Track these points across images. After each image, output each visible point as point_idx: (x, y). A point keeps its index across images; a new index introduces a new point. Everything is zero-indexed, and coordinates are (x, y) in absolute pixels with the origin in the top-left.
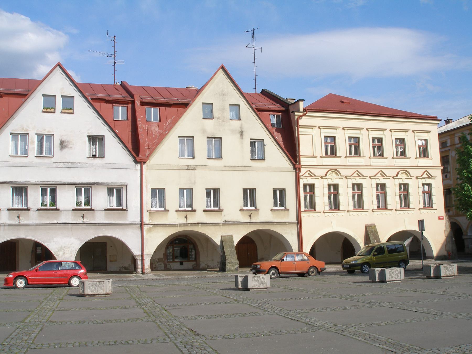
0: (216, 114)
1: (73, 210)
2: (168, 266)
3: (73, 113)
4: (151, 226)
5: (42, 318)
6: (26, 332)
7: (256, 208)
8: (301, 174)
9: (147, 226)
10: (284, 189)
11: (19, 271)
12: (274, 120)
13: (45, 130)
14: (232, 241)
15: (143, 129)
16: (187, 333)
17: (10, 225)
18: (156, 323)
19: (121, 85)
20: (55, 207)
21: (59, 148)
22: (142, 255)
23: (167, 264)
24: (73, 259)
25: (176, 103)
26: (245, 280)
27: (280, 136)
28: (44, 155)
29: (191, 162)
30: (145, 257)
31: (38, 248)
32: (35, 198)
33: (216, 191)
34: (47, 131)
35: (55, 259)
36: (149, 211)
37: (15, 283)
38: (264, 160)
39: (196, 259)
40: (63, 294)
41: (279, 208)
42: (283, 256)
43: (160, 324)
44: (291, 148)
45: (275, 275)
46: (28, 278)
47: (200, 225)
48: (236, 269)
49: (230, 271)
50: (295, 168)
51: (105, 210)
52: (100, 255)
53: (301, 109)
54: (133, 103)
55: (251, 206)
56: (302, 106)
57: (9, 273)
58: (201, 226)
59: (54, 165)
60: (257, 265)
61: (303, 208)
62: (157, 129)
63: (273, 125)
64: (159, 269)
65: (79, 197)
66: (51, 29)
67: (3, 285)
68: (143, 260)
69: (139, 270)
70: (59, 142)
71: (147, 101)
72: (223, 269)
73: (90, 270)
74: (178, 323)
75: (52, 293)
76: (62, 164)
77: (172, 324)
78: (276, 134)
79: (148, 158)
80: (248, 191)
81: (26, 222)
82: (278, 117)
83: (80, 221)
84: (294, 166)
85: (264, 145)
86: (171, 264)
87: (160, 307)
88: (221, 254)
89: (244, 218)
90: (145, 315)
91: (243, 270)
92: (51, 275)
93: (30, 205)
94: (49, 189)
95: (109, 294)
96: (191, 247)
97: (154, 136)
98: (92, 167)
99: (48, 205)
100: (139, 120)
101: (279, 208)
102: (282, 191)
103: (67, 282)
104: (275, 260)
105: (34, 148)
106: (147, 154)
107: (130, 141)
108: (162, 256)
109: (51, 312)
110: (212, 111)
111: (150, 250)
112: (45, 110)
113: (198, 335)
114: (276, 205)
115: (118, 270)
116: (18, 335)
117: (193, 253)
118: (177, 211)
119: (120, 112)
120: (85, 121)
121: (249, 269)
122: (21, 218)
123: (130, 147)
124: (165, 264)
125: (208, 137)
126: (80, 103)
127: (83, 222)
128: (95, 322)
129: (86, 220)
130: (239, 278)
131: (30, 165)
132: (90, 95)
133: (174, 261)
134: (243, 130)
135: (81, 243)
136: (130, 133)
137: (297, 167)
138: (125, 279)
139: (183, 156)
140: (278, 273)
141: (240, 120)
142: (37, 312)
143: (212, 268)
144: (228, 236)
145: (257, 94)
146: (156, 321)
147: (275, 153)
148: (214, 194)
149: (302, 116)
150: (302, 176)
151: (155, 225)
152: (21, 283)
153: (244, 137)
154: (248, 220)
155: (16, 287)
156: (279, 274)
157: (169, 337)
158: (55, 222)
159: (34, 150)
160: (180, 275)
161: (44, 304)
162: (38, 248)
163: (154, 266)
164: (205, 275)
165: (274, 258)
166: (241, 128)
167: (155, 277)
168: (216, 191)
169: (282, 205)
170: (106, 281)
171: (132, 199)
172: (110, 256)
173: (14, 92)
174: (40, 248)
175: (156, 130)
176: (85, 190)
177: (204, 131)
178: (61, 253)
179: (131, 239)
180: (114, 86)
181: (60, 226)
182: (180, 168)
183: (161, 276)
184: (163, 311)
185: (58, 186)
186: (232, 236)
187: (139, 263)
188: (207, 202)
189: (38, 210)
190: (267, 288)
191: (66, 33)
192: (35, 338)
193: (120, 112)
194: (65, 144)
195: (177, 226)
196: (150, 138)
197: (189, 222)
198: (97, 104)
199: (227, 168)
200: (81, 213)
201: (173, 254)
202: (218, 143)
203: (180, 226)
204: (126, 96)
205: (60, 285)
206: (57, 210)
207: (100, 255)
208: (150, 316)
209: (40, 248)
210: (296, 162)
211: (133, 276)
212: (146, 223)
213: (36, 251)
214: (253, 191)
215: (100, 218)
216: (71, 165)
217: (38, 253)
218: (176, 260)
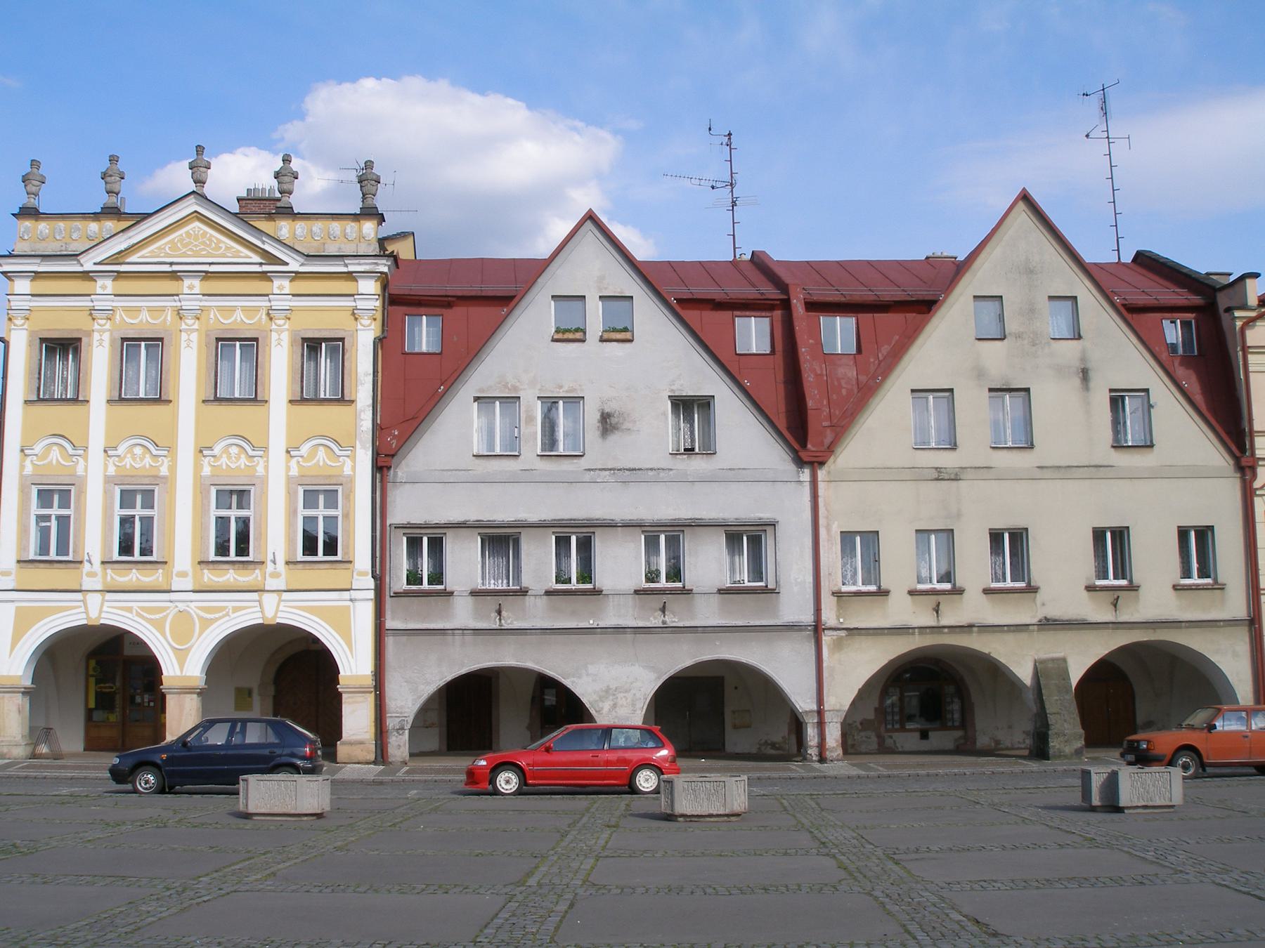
0: (1012, 326)
1: (637, 592)
2: (889, 742)
3: (631, 341)
4: (843, 633)
5: (570, 875)
6: (533, 910)
7: (1131, 581)
8: (1256, 485)
9: (831, 633)
10: (1211, 528)
11: (499, 750)
12: (1173, 332)
13: (561, 387)
14: (1065, 675)
15: (816, 375)
16: (963, 928)
17: (476, 631)
18: (876, 898)
19: (752, 260)
20: (679, 585)
21: (598, 433)
22: (820, 713)
23: (886, 735)
24: (638, 720)
25: (900, 301)
26: (1112, 784)
27: (1194, 378)
28: (561, 449)
29: (947, 460)
30: (828, 717)
31: (547, 691)
32: (539, 563)
33: (1019, 537)
34: (566, 388)
35: (591, 718)
36: (838, 594)
37: (492, 781)
38: (1151, 446)
39: (966, 722)
40: (617, 813)
41: (1195, 580)
42: (1215, 717)
43: (887, 900)
44: (1225, 409)
45: (1191, 771)
46: (527, 768)
48: (1078, 752)
49: (1059, 757)
50: (1240, 468)
51: (721, 591)
52: (708, 709)
53: (1252, 300)
54: (786, 305)
55: (1115, 578)
56: (1254, 291)
57: (479, 755)
58: (979, 632)
59: (588, 476)
60: (1138, 741)
62: (852, 373)
63: (1173, 347)
64: (863, 748)
65: (653, 559)
66: (580, 124)
67: (461, 787)
68: (821, 725)
69: (813, 752)
70: (598, 416)
71: (822, 299)
72: (1040, 750)
73: (688, 749)
74: (934, 899)
75: (588, 810)
77: (919, 903)
78: (1180, 372)
79: (831, 449)
80: (1108, 535)
81: (516, 625)
82: (1186, 325)
83: (655, 620)
84: (1237, 460)
85: (1150, 406)
86: (895, 735)
87: (879, 852)
88: (1035, 708)
89: (1098, 612)
90: (843, 874)
91: (1096, 755)
92: (586, 763)
93: (526, 581)
94: (425, 540)
95: (738, 815)
96: (950, 689)
97: (844, 392)
99: (574, 579)
100: (803, 350)
101: (1195, 580)
102: (1205, 534)
103: (626, 781)
104: (1191, 727)
106: (827, 441)
107: (782, 407)
108: (870, 715)
109: (592, 861)
110: (1001, 318)
111: (841, 696)
112: (559, 336)
113: (995, 934)
114: (1187, 573)
115: (754, 751)
116: (514, 920)
117: (956, 706)
118: (912, 593)
119: (753, 334)
120: (665, 356)
121: (1115, 754)
122: (504, 613)
123: (782, 424)
124: (879, 736)
125: (991, 390)
126: (649, 316)
127: (664, 622)
128: (709, 890)
129: (672, 620)
130: (1094, 777)
131: (526, 478)
132: (676, 290)
133: (903, 729)
134: (1089, 365)
135: (659, 678)
136: (781, 387)
138: (775, 775)
139: (924, 443)
140: (1201, 764)
141: (1080, 337)
142: (555, 858)
143: (1007, 749)
144: (1053, 660)
145: (1124, 264)
146: (876, 893)
147: (1181, 429)
148: (1011, 544)
149: (1253, 320)
151: (853, 631)
152: (507, 782)
153: (1092, 384)
154: (1106, 615)
155: (496, 792)
156: (1203, 765)
157: (915, 938)
158: (591, 623)
160: (922, 766)
161: (570, 837)
162: (547, 691)
163: (850, 742)
164: (991, 769)
165: (1187, 722)
167: (855, 772)
168: (1019, 537)
169: (1203, 573)
170: (731, 781)
171: (790, 563)
172: (734, 712)
173: (479, 294)
174: (554, 691)
175: (850, 375)
176: (668, 536)
177: (980, 373)
178: (606, 706)
179: (788, 670)
180: (734, 263)
182: (917, 475)
183: (870, 769)
184: (890, 865)
185: (598, 531)
186: (1064, 660)
187: (811, 733)
188: (994, 568)
189: (549, 593)
190: (1172, 806)
191: (615, 132)
192: (557, 929)
193: (753, 334)
194: (614, 420)
195: (971, 632)
196: (835, 397)
197: (944, 622)
198: (691, 315)
199: (1047, 474)
200: (657, 601)
201: (902, 709)
202: (944, 404)
203: (920, 633)
204: (769, 288)
205: (606, 789)
206: (596, 592)
207: (708, 709)
208: (855, 879)
209: (554, 691)
210: (1242, 449)
211: (795, 768)
212: (828, 625)
214: (1121, 535)
215: (708, 613)
216: (629, 475)
217: (547, 703)
218: (909, 726)
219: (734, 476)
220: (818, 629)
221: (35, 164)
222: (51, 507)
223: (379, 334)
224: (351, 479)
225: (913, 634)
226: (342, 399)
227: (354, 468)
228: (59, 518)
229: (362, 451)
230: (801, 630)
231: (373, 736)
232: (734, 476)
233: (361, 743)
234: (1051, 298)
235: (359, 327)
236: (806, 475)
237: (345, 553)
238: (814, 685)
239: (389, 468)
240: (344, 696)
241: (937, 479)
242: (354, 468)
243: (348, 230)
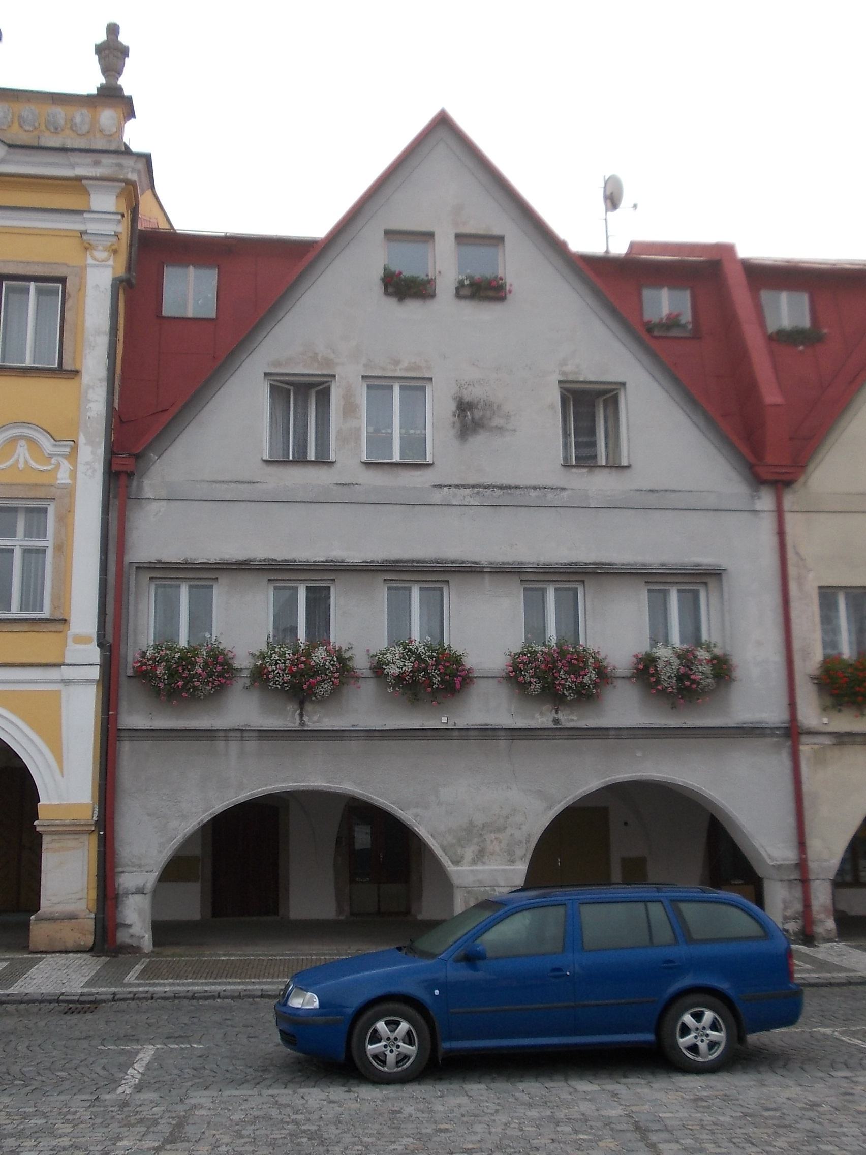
4: (827, 741)
17: (264, 734)
22: (802, 866)
34: (405, 364)
59: (437, 497)
70: (453, 406)
76: (468, 491)
98: (581, 506)
105: (359, 429)
159: (358, 438)
181: (467, 738)
213: (351, 839)
216: (503, 496)
217: (358, 846)
219: (654, 502)
220: (792, 732)
221: (113, 30)
222: (13, 534)
223: (121, 272)
224: (70, 492)
226: (65, 372)
227: (73, 474)
228: (27, 551)
229: (89, 449)
231: (93, 905)
232: (654, 502)
233: (72, 917)
235: (90, 261)
236: (766, 501)
237: (55, 607)
238: (791, 821)
239: (130, 475)
240: (46, 839)
242: (73, 474)
243: (78, 119)
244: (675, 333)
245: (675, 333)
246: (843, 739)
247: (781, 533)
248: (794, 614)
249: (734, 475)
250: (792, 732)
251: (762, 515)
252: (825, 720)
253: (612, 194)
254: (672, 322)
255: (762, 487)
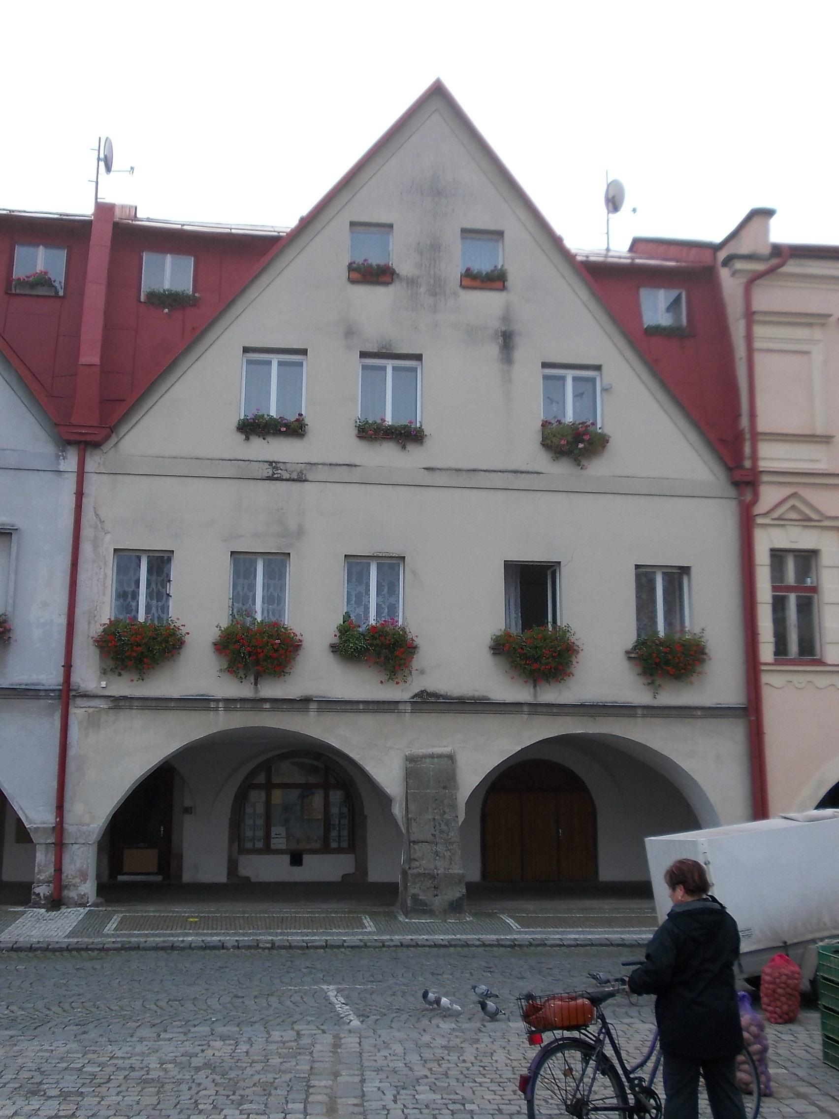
4: (103, 704)
8: (763, 506)
22: (59, 829)
47: (526, 709)
58: (320, 710)
61: (767, 652)
68: (60, 846)
102: (677, 577)
137: (743, 480)
150: (766, 514)
153: (519, 354)
166: (506, 318)
186: (451, 757)
195: (306, 710)
203: (226, 709)
210: (738, 457)
220: (66, 695)
225: (216, 709)
230: (38, 697)
234: (464, 231)
236: (70, 463)
238: (55, 784)
241: (270, 479)
244: (41, 291)
245: (41, 291)
246: (119, 703)
247: (80, 494)
248: (83, 575)
249: (42, 435)
250: (66, 695)
251: (66, 475)
252: (103, 684)
253: (613, 197)
254: (43, 281)
255: (69, 447)
